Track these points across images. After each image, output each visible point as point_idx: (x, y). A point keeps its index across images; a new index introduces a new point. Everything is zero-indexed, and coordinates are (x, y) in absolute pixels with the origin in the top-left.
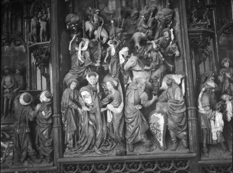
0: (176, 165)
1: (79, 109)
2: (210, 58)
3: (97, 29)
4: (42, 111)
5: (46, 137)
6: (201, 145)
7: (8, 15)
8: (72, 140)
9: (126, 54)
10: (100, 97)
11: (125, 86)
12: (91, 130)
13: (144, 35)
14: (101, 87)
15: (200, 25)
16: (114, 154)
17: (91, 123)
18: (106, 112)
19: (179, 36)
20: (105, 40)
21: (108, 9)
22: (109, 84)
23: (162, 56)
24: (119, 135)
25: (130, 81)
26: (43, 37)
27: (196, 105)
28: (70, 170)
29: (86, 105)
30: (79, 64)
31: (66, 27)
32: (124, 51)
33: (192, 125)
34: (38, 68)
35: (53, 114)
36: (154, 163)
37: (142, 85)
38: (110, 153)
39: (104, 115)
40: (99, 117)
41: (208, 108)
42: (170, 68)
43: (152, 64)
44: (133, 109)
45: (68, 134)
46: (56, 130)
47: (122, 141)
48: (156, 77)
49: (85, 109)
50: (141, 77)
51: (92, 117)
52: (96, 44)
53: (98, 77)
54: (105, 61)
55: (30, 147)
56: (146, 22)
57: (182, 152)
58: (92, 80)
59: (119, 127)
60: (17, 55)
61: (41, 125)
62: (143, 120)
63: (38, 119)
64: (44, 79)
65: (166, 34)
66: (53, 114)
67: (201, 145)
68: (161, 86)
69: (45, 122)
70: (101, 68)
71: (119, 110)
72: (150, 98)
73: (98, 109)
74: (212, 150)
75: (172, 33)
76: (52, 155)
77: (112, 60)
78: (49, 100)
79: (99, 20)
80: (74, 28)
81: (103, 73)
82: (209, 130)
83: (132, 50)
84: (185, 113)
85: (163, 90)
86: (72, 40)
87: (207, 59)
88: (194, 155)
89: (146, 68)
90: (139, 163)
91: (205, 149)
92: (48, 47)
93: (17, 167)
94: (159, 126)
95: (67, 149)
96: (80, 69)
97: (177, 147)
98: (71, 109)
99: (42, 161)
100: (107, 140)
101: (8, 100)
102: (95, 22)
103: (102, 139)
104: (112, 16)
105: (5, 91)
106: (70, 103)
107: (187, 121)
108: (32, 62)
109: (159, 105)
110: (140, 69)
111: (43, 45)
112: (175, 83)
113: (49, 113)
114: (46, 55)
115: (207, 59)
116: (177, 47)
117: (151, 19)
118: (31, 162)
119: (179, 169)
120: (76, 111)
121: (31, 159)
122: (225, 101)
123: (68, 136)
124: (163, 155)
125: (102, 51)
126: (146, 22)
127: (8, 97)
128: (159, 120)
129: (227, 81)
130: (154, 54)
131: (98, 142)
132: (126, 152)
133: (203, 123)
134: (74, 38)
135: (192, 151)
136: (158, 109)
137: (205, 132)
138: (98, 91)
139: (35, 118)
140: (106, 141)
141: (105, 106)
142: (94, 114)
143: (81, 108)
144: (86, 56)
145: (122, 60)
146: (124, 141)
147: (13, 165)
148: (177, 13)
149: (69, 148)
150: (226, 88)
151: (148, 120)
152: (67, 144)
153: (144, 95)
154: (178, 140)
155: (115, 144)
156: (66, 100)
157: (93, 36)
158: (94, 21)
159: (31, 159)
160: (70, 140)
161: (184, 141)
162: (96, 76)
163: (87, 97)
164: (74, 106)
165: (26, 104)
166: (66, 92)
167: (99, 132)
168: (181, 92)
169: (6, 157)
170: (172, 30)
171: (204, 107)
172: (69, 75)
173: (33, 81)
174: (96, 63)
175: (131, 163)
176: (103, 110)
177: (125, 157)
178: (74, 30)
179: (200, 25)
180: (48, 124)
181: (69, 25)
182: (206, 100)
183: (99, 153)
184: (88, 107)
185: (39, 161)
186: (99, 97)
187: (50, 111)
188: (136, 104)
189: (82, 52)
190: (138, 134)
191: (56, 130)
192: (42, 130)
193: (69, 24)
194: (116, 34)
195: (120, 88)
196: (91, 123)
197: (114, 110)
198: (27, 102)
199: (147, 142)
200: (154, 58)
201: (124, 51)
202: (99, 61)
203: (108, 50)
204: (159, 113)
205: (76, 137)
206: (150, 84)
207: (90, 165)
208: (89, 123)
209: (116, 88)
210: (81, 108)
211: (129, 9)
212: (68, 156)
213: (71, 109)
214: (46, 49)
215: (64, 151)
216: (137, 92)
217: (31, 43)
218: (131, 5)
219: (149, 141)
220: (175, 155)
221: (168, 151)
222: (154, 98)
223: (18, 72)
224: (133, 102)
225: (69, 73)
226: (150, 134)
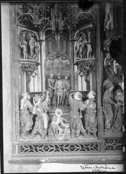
1: (115, 104)
4: (90, 105)
5: (93, 121)
7: (58, 38)
26: (89, 56)
28: (109, 143)
30: (114, 74)
31: (103, 49)
34: (79, 76)
35: (97, 106)
45: (108, 120)
49: (119, 104)
60: (63, 66)
63: (88, 110)
66: (97, 106)
69: (93, 111)
78: (94, 97)
80: (108, 50)
86: (107, 58)
92: (92, 62)
93: (74, 140)
96: (114, 77)
101: (60, 97)
105: (59, 90)
111: (88, 61)
113: (94, 106)
127: (60, 95)
134: (108, 57)
139: (86, 109)
144: (119, 69)
147: (72, 139)
149: (108, 129)
160: (109, 123)
169: (66, 133)
173: (76, 84)
178: (108, 51)
187: (95, 104)
189: (116, 66)
193: (106, 47)
210: (116, 103)
214: (90, 63)
217: (79, 58)
220: (17, 159)
223: (66, 78)
225: (106, 80)
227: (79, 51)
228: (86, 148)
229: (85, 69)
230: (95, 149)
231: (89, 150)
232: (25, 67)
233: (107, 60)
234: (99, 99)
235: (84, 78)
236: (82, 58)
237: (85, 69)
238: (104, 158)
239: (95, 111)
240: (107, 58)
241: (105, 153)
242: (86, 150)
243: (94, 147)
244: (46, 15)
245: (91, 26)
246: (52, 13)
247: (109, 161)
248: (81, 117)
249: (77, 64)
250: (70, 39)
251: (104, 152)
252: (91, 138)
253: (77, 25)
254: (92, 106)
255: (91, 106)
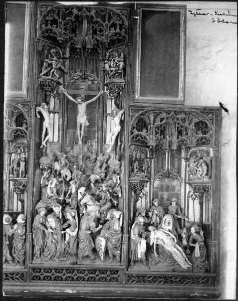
0: (111, 274)
1: (46, 230)
2: (146, 196)
3: (63, 169)
5: (20, 248)
6: (129, 261)
8: (39, 252)
9: (83, 192)
10: (62, 222)
11: (81, 215)
12: (53, 246)
13: (98, 177)
14: (62, 214)
15: (138, 176)
16: (68, 263)
17: (53, 241)
18: (65, 234)
19: (122, 182)
20: (68, 179)
21: (73, 152)
22: (70, 214)
23: (109, 195)
24: (73, 250)
25: (84, 211)
26: (22, 175)
27: (129, 233)
29: (51, 228)
32: (82, 190)
33: (125, 247)
36: (96, 271)
37: (92, 217)
38: (66, 262)
39: (64, 236)
40: (59, 237)
41: (137, 236)
42: (114, 203)
43: (101, 201)
44: (84, 234)
46: (28, 245)
47: (75, 255)
48: (103, 210)
49: (50, 230)
50: (93, 209)
51: (55, 237)
52: (61, 182)
53: (61, 207)
54: (67, 196)
55: (8, 254)
56: (101, 167)
57: (115, 265)
58: (57, 210)
59: (74, 245)
61: (17, 240)
62: (90, 241)
64: (20, 203)
65: (114, 179)
66: (26, 232)
67: (129, 261)
68: (106, 217)
69: (20, 237)
70: (64, 200)
71: (75, 234)
72: (97, 227)
73: (59, 231)
74: (137, 264)
75: (118, 178)
76: (24, 261)
77: (72, 196)
78: (24, 222)
79: (65, 162)
81: (64, 204)
82: (136, 252)
83: (88, 188)
84: (120, 239)
85: (107, 220)
86: (44, 176)
87: (144, 197)
88: (123, 267)
89: (97, 203)
90: (85, 270)
91: (132, 263)
94: (101, 246)
95: (35, 257)
97: (113, 260)
98: (40, 230)
99: (16, 265)
100: (65, 253)
102: (62, 164)
103: (61, 252)
104: (75, 158)
106: (40, 225)
107: (121, 244)
108: (11, 188)
109: (103, 231)
110: (92, 203)
112: (115, 217)
114: (23, 187)
115: (144, 197)
116: (120, 190)
117: (105, 165)
118: (8, 265)
119: (112, 276)
120: (44, 232)
121: (8, 263)
122: (150, 232)
123: (37, 248)
124: (102, 266)
125: (65, 188)
126: (101, 167)
128: (101, 242)
129: (155, 216)
130: (103, 194)
131: (58, 254)
132: (77, 262)
133: (132, 246)
135: (122, 264)
136: (102, 234)
137: (133, 252)
138: (61, 217)
139: (13, 234)
140: (64, 253)
141: (64, 229)
142: (57, 234)
143: (47, 230)
145: (80, 197)
146: (77, 255)
148: (123, 165)
149: (37, 257)
150: (153, 221)
151: (94, 241)
152: (36, 254)
153: (93, 224)
154: (114, 256)
155: (70, 256)
156: (36, 223)
157: (60, 174)
158: (61, 163)
159: (8, 263)
160: (38, 251)
161: (118, 258)
162: (59, 207)
163: (52, 222)
164: (42, 228)
165: (7, 223)
166: (37, 217)
167: (58, 247)
168: (119, 224)
170: (118, 177)
171: (135, 235)
172: (40, 204)
174: (61, 197)
175: (80, 270)
176: (63, 232)
177: (75, 266)
179: (138, 176)
180: (22, 239)
181: (42, 166)
182: (136, 231)
183: (58, 261)
184: (52, 229)
185: (15, 264)
186: (60, 223)
187: (25, 230)
188: (87, 229)
189: (50, 188)
190: (86, 251)
191: (28, 245)
192: (17, 243)
194: (77, 176)
195: (76, 217)
196: (53, 241)
197: (71, 233)
198: (7, 222)
199: (92, 257)
200: (103, 197)
201: (82, 190)
202: (62, 196)
203: (70, 188)
204: (102, 237)
205: (42, 251)
206: (99, 215)
207: (51, 270)
208: (52, 241)
209: (74, 217)
211: (89, 154)
212: (35, 262)
213: (40, 230)
215: (33, 259)
216: (88, 223)
218: (91, 150)
219: (94, 256)
221: (107, 263)
222: (100, 226)
224: (85, 229)
226: (94, 251)
227: (13, 168)
228: (11, 277)
229: (19, 189)
230: (21, 278)
231: (13, 280)
232: (44, 86)
233: (44, 178)
234: (28, 225)
235: (113, 101)
236: (16, 176)
237: (19, 189)
238: (27, 290)
239: (24, 237)
240: (44, 176)
241: (31, 284)
242: (11, 279)
243: (20, 277)
244: (71, 31)
245: (26, 141)
246: (77, 30)
247: (189, 108)
248: (6, 243)
249: (107, 85)
250: (101, 59)
251: (30, 282)
252: (17, 266)
253: (109, 43)
254: (20, 231)
255: (19, 231)
